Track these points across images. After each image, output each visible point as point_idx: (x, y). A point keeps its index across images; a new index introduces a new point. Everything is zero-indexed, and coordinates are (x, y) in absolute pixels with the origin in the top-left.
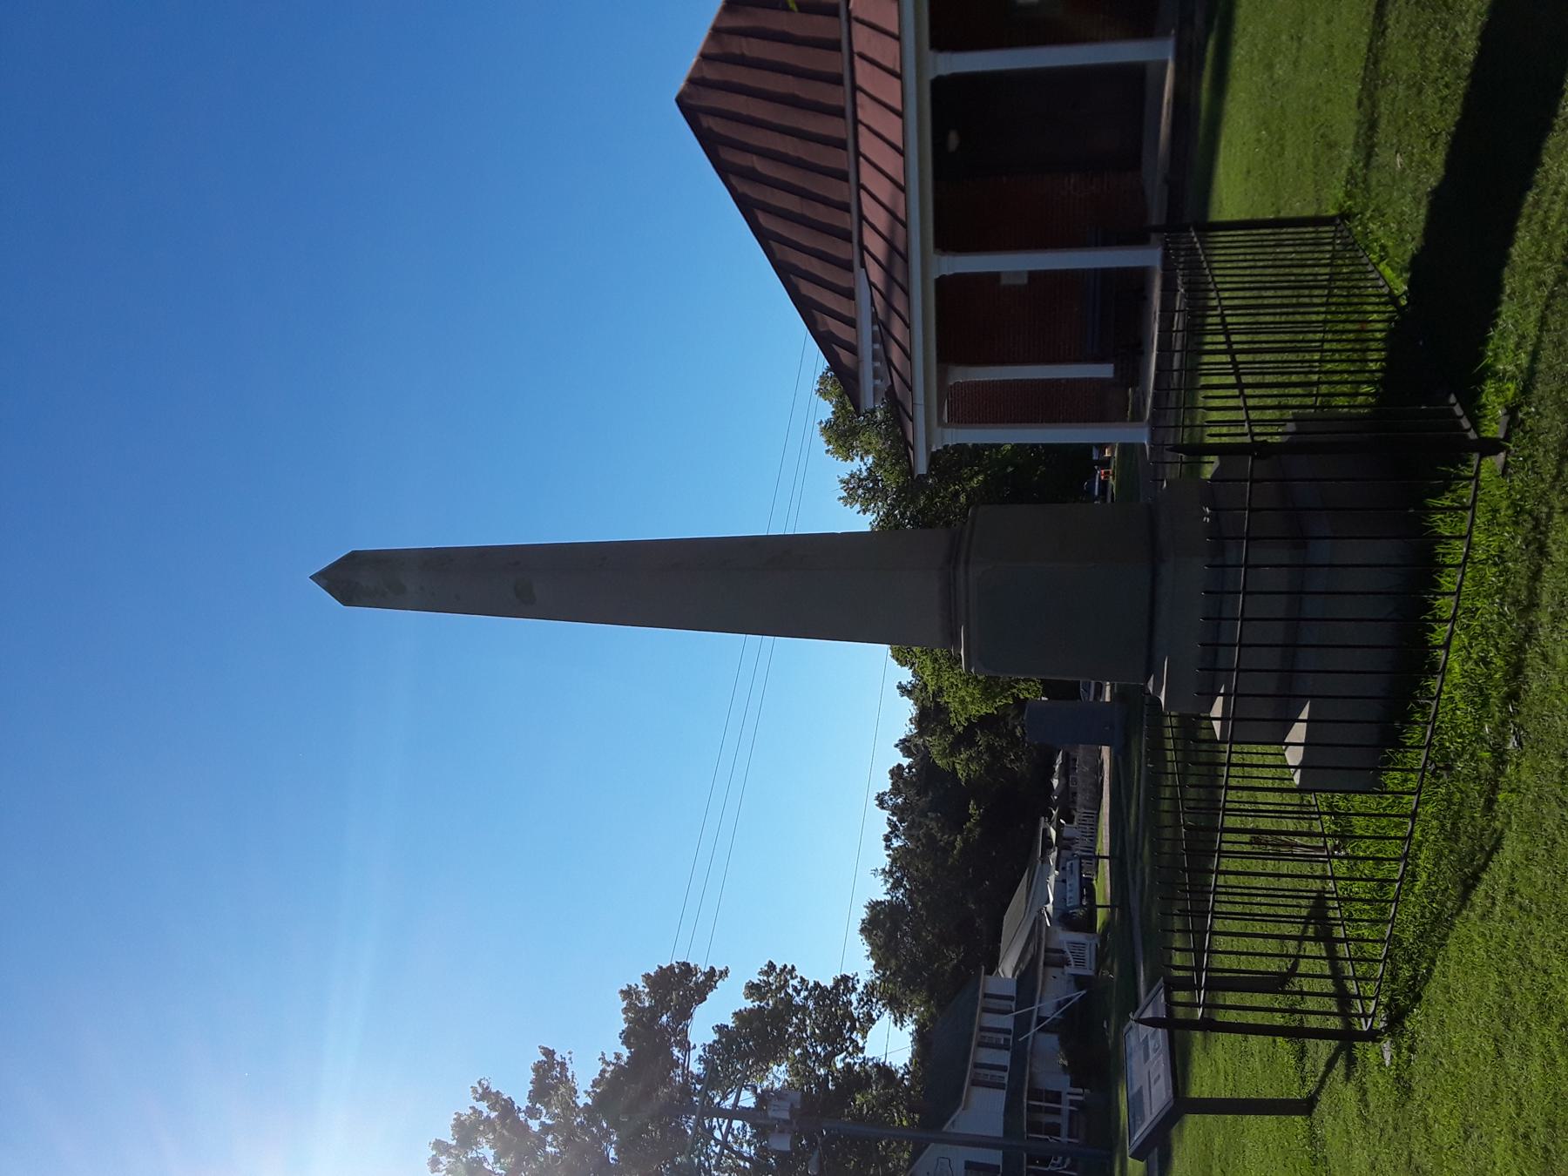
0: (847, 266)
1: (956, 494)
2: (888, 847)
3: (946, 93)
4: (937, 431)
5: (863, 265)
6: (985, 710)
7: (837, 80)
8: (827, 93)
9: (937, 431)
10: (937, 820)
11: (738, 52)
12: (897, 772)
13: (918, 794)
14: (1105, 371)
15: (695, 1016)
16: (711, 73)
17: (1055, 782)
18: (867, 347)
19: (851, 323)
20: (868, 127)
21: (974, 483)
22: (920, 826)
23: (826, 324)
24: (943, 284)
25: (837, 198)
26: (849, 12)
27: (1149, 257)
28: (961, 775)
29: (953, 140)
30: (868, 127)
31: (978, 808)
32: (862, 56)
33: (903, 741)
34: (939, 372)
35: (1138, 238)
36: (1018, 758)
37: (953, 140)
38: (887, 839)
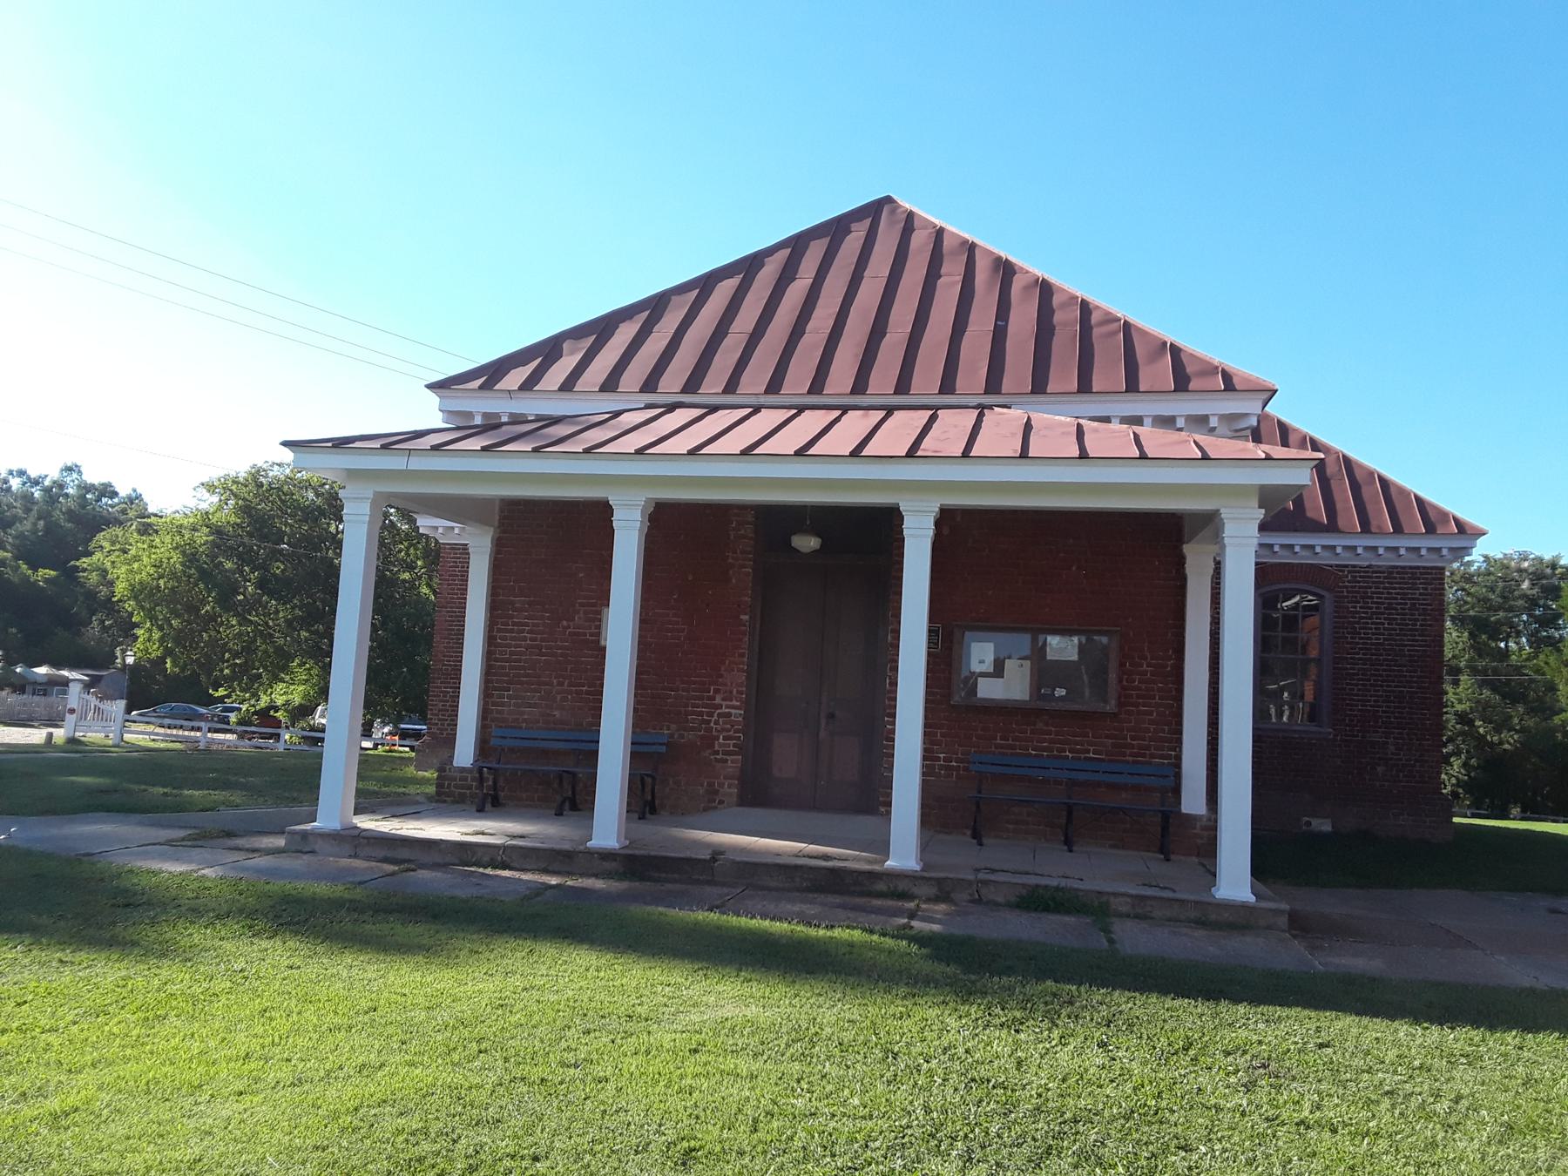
0: (650, 385)
1: (411, 567)
2: (11, 473)
3: (875, 531)
4: (368, 490)
5: (649, 407)
6: (121, 588)
7: (903, 386)
8: (886, 372)
9: (368, 490)
10: (34, 531)
11: (943, 271)
12: (107, 491)
13: (70, 512)
14: (464, 753)
15: (255, 446)
16: (919, 240)
17: (42, 670)
18: (532, 406)
19: (568, 386)
20: (837, 420)
21: (425, 590)
22: (28, 510)
23: (572, 353)
24: (603, 511)
25: (745, 378)
26: (991, 407)
27: (607, 826)
28: (84, 562)
29: (807, 543)
30: (837, 420)
31: (46, 581)
32: (933, 419)
33: (139, 497)
34: (486, 502)
35: (644, 800)
36: (105, 629)
37: (807, 543)
38: (21, 473)
